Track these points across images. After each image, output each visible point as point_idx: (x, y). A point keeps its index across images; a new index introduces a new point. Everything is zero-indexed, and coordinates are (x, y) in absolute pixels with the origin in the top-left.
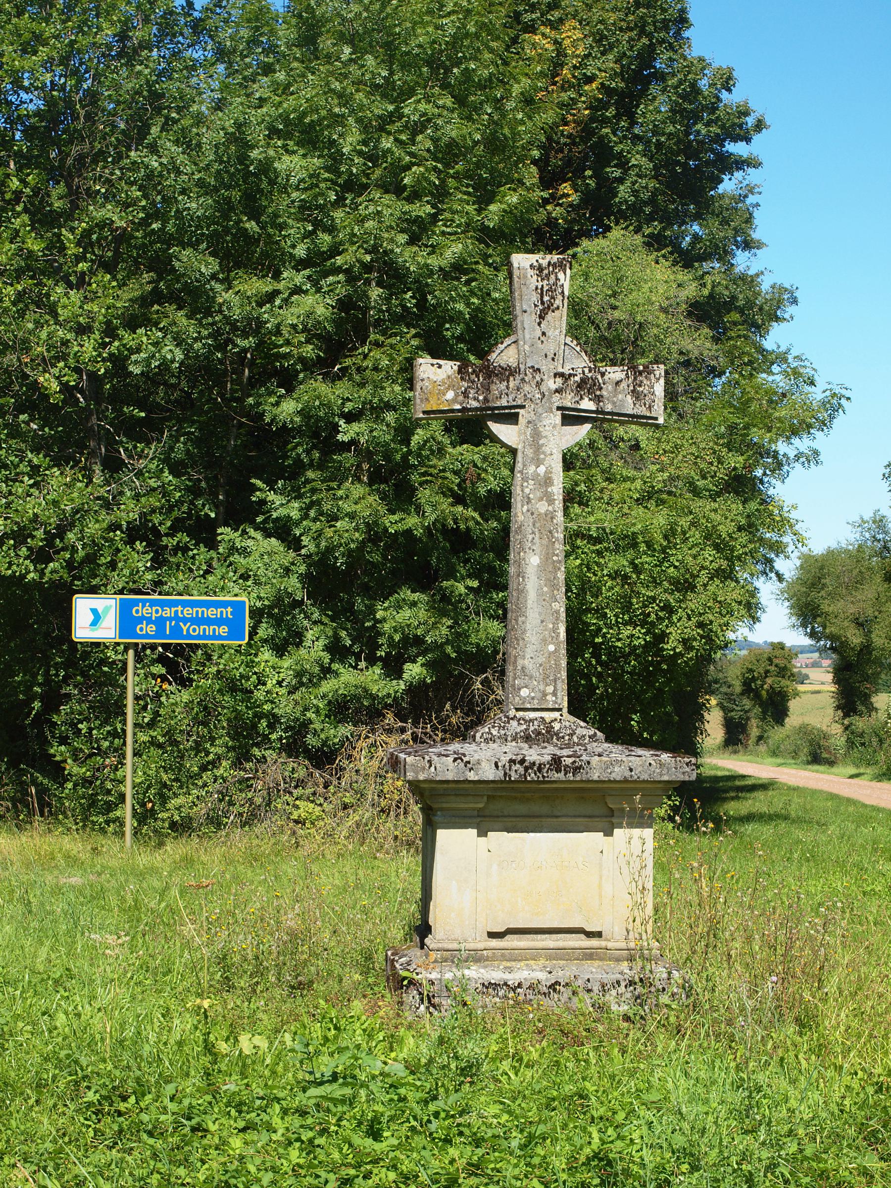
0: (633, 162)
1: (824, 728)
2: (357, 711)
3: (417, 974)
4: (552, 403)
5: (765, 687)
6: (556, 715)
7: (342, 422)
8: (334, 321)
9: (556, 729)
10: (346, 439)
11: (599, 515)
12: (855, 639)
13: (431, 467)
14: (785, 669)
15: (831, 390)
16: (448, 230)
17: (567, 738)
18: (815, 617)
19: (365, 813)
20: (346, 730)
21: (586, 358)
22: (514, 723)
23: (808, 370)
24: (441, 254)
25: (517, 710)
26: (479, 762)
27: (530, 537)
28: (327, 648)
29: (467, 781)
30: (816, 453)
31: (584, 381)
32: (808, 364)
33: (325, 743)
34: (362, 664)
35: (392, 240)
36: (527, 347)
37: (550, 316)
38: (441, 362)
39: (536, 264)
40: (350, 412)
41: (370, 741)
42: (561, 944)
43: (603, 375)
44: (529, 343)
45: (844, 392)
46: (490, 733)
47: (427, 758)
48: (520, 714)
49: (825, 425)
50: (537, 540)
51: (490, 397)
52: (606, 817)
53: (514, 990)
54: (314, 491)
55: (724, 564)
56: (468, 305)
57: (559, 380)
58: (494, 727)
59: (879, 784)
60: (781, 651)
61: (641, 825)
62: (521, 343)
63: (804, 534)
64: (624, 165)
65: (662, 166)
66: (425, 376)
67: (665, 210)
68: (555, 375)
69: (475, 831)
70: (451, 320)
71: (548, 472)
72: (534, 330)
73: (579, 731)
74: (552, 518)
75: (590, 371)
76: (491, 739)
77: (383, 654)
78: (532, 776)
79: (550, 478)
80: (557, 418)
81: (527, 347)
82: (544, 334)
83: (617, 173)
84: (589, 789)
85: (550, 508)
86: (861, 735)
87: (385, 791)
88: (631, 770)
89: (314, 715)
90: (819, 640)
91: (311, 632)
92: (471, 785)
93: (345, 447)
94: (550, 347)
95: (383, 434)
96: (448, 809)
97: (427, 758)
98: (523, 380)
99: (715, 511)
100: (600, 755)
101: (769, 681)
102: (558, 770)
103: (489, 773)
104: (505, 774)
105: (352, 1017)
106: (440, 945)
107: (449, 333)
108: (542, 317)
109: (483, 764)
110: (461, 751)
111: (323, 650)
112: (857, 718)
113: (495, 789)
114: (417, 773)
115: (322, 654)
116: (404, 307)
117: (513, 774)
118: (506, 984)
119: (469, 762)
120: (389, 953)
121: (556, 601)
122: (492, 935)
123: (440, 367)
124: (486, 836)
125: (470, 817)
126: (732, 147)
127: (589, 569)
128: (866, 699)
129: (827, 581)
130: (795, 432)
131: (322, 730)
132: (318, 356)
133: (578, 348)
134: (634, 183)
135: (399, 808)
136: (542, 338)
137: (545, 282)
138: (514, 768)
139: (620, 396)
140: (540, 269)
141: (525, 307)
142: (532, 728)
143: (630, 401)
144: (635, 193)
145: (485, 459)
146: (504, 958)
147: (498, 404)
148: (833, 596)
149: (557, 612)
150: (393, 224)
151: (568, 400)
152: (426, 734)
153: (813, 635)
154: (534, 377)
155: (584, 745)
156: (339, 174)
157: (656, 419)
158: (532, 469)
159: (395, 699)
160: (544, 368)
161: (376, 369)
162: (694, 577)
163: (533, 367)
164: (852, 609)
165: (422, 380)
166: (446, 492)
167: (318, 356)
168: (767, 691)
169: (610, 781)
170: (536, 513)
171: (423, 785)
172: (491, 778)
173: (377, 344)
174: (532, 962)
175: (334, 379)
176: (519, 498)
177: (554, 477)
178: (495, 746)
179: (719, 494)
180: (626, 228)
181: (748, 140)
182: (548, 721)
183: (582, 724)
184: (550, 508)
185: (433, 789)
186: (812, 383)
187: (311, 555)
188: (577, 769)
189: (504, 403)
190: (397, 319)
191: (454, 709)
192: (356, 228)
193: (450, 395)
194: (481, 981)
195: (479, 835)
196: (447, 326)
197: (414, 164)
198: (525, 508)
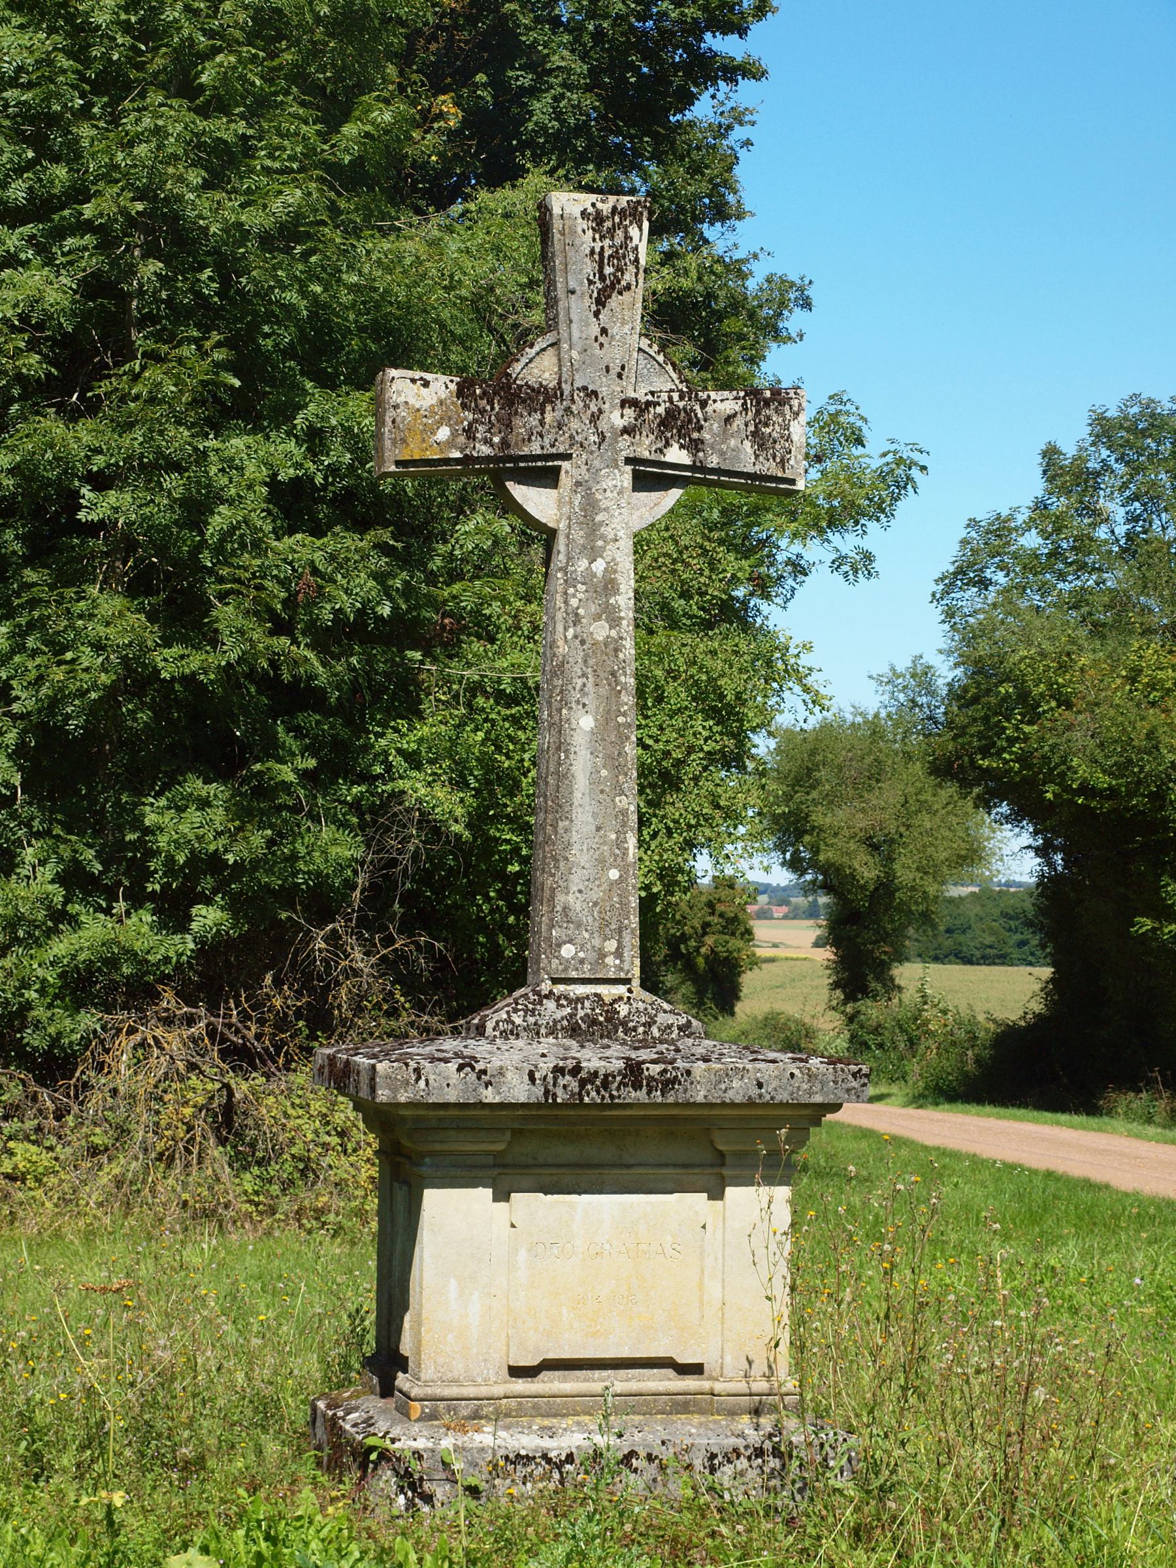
0: (556, 61)
1: (807, 1020)
2: (113, 987)
3: (393, 1441)
4: (617, 452)
5: (703, 950)
6: (621, 990)
7: (85, 491)
8: (74, 314)
9: (623, 1014)
10: (94, 517)
11: (515, 657)
12: (867, 870)
13: (239, 567)
14: (735, 920)
15: (895, 452)
16: (277, 165)
17: (641, 1030)
18: (800, 834)
19: (125, 1164)
20: (89, 1020)
21: (674, 376)
22: (550, 1005)
23: (852, 419)
24: (265, 206)
25: (555, 981)
26: (501, 1072)
27: (579, 682)
28: (59, 879)
29: (482, 1105)
30: (868, 557)
31: (672, 413)
32: (852, 409)
33: (55, 1040)
34: (120, 906)
35: (181, 179)
36: (574, 354)
37: (615, 301)
38: (428, 376)
39: (590, 210)
40: (100, 471)
41: (138, 1037)
42: (634, 1386)
43: (704, 404)
44: (579, 346)
45: (916, 456)
46: (509, 1021)
47: (413, 1064)
48: (560, 989)
49: (883, 511)
50: (590, 687)
51: (512, 439)
52: (712, 1166)
53: (559, 1466)
54: (34, 603)
55: (731, 743)
56: (303, 293)
57: (630, 412)
58: (516, 1011)
59: (921, 1112)
60: (728, 891)
61: (770, 1181)
62: (566, 346)
63: (823, 691)
64: (539, 68)
65: (602, 70)
66: (395, 399)
67: (604, 145)
68: (624, 403)
69: (489, 1192)
70: (270, 317)
71: (611, 570)
72: (588, 325)
73: (661, 1018)
74: (616, 650)
75: (681, 398)
76: (511, 1032)
77: (157, 887)
78: (592, 1096)
79: (613, 581)
80: (625, 477)
81: (574, 354)
82: (604, 331)
83: (526, 80)
84: (687, 1119)
85: (613, 633)
86: (877, 1030)
87: (163, 1123)
88: (760, 1085)
89: (34, 995)
90: (803, 873)
91: (30, 850)
92: (487, 1112)
93: (93, 529)
94: (614, 355)
95: (162, 511)
96: (451, 1153)
97: (413, 1064)
98: (568, 410)
99: (713, 653)
100: (706, 1060)
101: (709, 940)
102: (637, 1086)
103: (518, 1090)
104: (547, 1092)
105: (300, 1518)
106: (429, 1391)
107: (269, 343)
108: (601, 302)
109: (509, 1075)
110: (467, 1052)
111: (52, 882)
112: (869, 1002)
113: (526, 1118)
114: (395, 1090)
115: (50, 888)
116: (198, 295)
117: (560, 1092)
118: (545, 1456)
119: (484, 1072)
120: (321, 1405)
121: (622, 793)
122: (516, 1372)
123: (426, 384)
124: (507, 1199)
125: (483, 1167)
126: (715, 42)
127: (499, 749)
128: (882, 972)
129: (822, 774)
130: (834, 521)
131: (51, 1019)
132: (49, 375)
133: (661, 358)
134: (557, 99)
135: (190, 1152)
136: (601, 339)
137: (607, 242)
138: (561, 1081)
139: (733, 442)
140: (599, 219)
141: (572, 284)
142: (581, 1013)
143: (750, 451)
144: (558, 115)
145: (332, 558)
146: (538, 1412)
147: (526, 451)
148: (832, 800)
149: (624, 812)
150: (180, 152)
151: (644, 447)
152: (230, 1026)
153: (795, 865)
154: (587, 406)
155: (672, 1043)
156: (87, 62)
157: (792, 482)
158: (583, 564)
159: (179, 967)
160: (603, 391)
161: (152, 400)
162: (679, 763)
163: (585, 388)
164: (862, 822)
165: (396, 407)
166: (262, 612)
167: (49, 375)
168: (706, 958)
169: (724, 1104)
170: (589, 641)
171: (403, 1112)
172: (523, 1099)
173: (153, 357)
174: (586, 1418)
175: (72, 416)
176: (560, 615)
177: (621, 580)
178: (520, 1043)
179: (708, 625)
180: (551, 173)
181: (742, 32)
182: (607, 1000)
183: (666, 1006)
184: (613, 633)
185: (418, 1119)
186: (859, 441)
187: (29, 714)
188: (668, 1084)
189: (535, 448)
190: (179, 314)
191: (278, 983)
192: (120, 156)
193: (443, 433)
194: (502, 1452)
195: (496, 1199)
196: (266, 329)
197: (219, 50)
198: (570, 633)
